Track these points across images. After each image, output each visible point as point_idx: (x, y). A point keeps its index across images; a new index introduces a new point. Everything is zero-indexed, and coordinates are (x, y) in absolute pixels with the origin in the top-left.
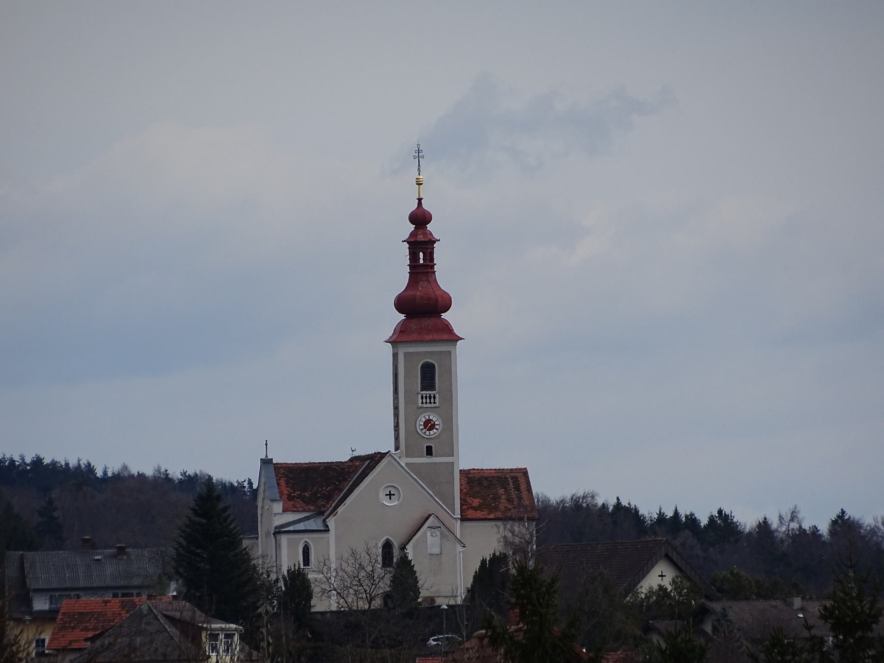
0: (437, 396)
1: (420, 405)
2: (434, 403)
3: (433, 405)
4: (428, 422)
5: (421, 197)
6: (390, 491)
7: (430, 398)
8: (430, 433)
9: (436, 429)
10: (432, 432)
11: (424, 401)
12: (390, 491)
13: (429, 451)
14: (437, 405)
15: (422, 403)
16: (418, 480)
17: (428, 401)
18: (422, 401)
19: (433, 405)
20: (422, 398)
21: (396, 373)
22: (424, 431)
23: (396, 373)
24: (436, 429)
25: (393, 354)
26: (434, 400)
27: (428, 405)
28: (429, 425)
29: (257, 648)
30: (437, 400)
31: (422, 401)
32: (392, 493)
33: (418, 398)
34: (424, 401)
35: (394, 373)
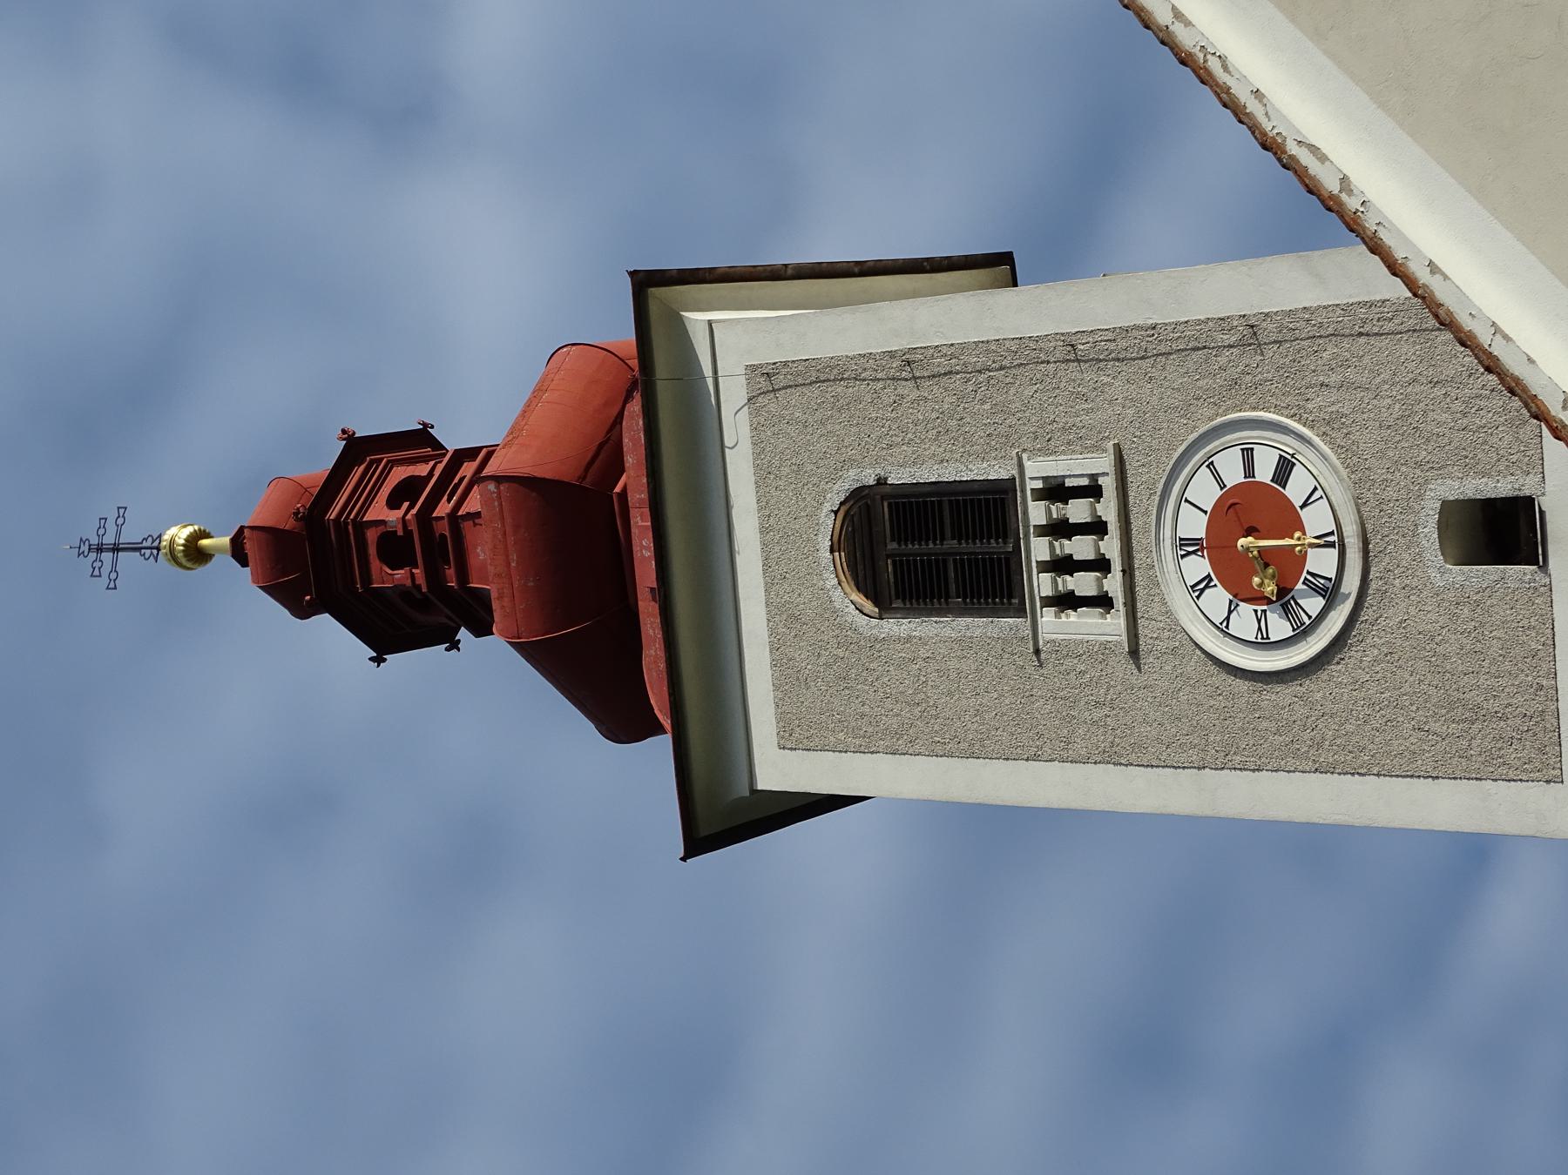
0: (1038, 469)
11: (1082, 584)
20: (1066, 601)
34: (1082, 584)
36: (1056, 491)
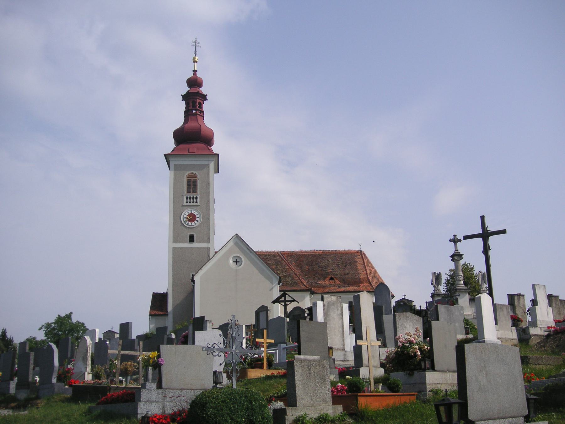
0: (198, 197)
1: (185, 204)
2: (196, 202)
3: (195, 204)
4: (190, 220)
5: (196, 69)
6: (236, 260)
7: (193, 198)
8: (191, 224)
9: (197, 221)
10: (193, 224)
11: (189, 200)
12: (236, 260)
13: (192, 239)
14: (198, 204)
15: (187, 202)
16: (405, 393)
17: (192, 200)
18: (187, 201)
19: (195, 204)
20: (187, 198)
21: (452, 371)
22: (185, 220)
23: (452, 371)
24: (197, 221)
25: (521, 357)
26: (196, 200)
27: (192, 204)
28: (192, 218)
29: (226, 338)
30: (198, 200)
31: (187, 201)
32: (237, 261)
33: (183, 199)
34: (189, 200)
35: (353, 329)
36: (196, 198)
